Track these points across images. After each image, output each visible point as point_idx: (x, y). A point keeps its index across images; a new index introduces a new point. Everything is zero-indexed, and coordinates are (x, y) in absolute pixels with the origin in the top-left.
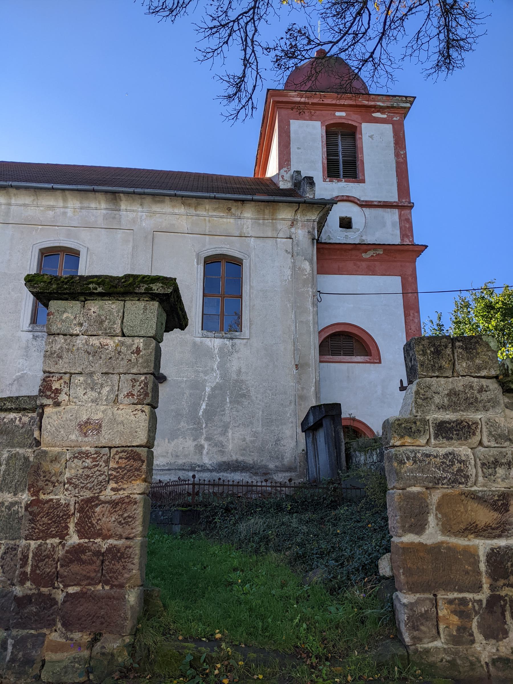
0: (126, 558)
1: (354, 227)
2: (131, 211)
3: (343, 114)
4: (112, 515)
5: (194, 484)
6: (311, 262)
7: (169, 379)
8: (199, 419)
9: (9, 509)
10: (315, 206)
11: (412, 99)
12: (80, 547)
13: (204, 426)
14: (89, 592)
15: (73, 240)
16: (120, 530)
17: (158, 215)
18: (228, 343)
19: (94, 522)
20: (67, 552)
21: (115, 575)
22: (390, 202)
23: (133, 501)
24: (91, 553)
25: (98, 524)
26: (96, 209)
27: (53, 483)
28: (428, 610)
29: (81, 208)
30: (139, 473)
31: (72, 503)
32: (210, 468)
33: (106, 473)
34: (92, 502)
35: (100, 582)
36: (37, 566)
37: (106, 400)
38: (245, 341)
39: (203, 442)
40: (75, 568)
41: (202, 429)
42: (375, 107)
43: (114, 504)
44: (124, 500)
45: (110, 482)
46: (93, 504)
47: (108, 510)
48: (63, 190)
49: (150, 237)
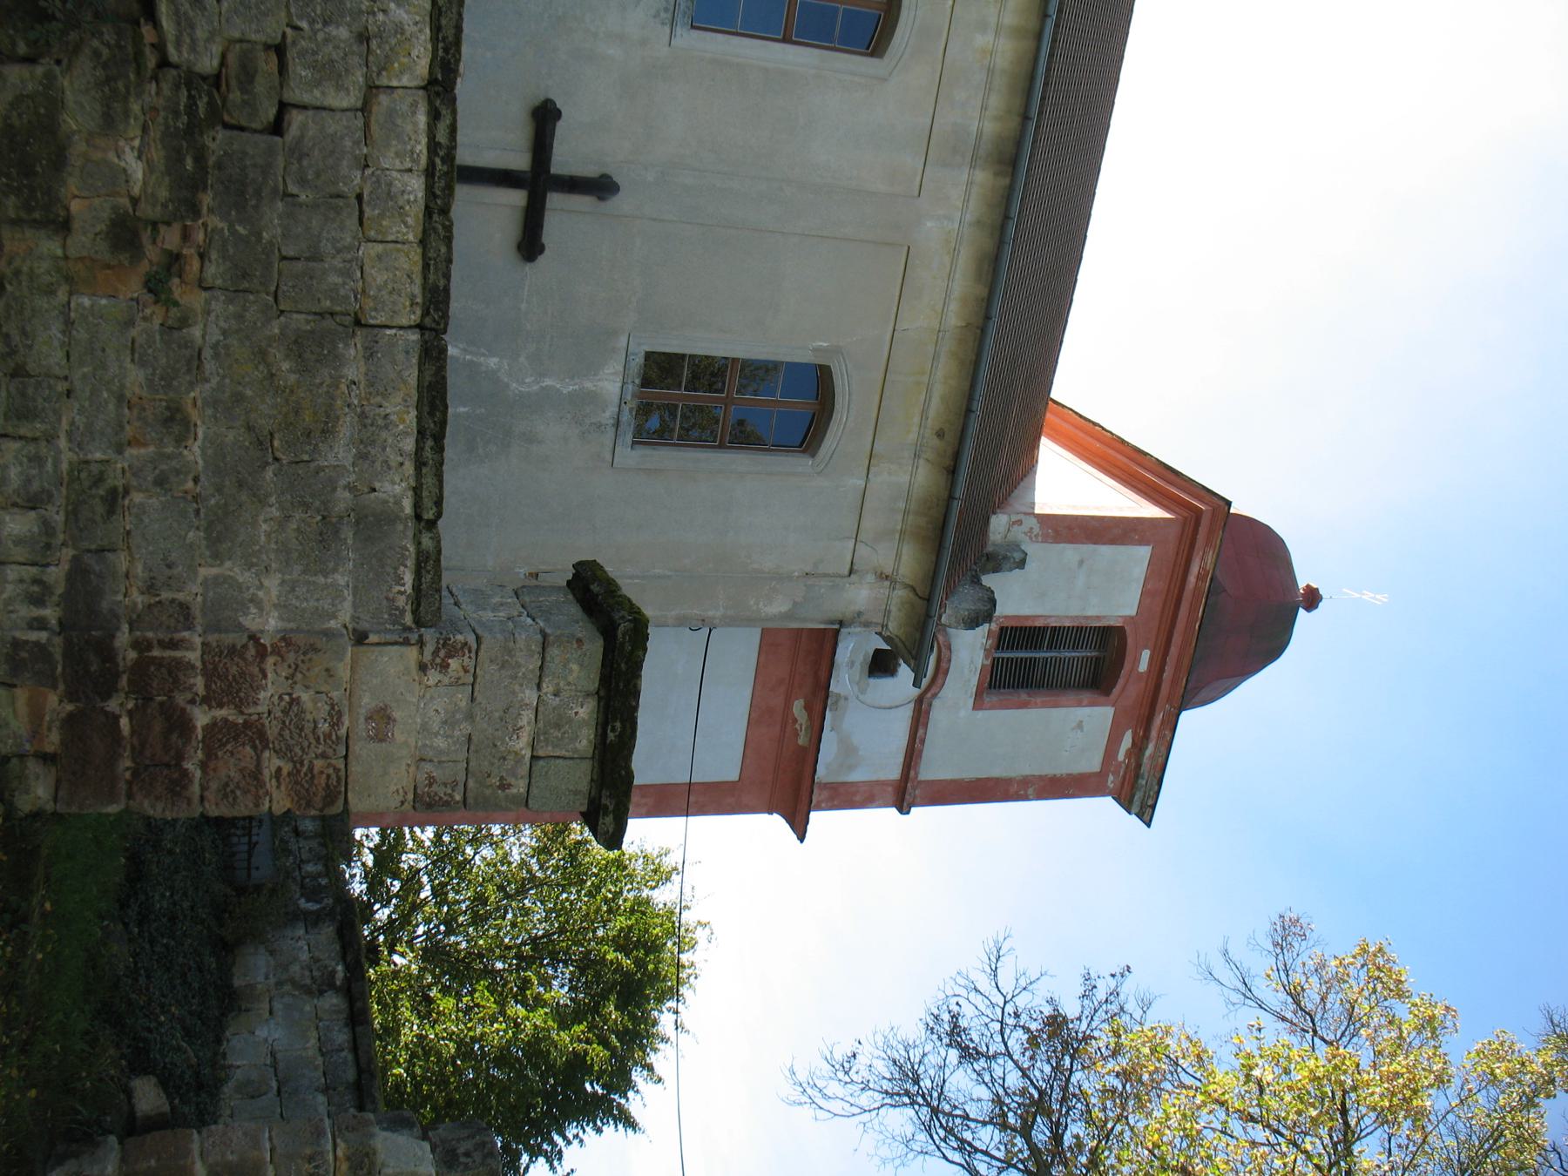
1: (872, 681)
2: (968, 193)
3: (1143, 666)
6: (787, 616)
7: (528, 267)
9: (251, 601)
10: (918, 635)
11: (1146, 817)
16: (214, 786)
17: (947, 260)
18: (608, 414)
20: (183, 710)
22: (917, 765)
26: (984, 108)
27: (293, 676)
29: (990, 71)
31: (260, 709)
36: (161, 665)
37: (425, 745)
38: (608, 457)
40: (158, 726)
42: (1146, 737)
43: (256, 775)
48: (1039, 37)
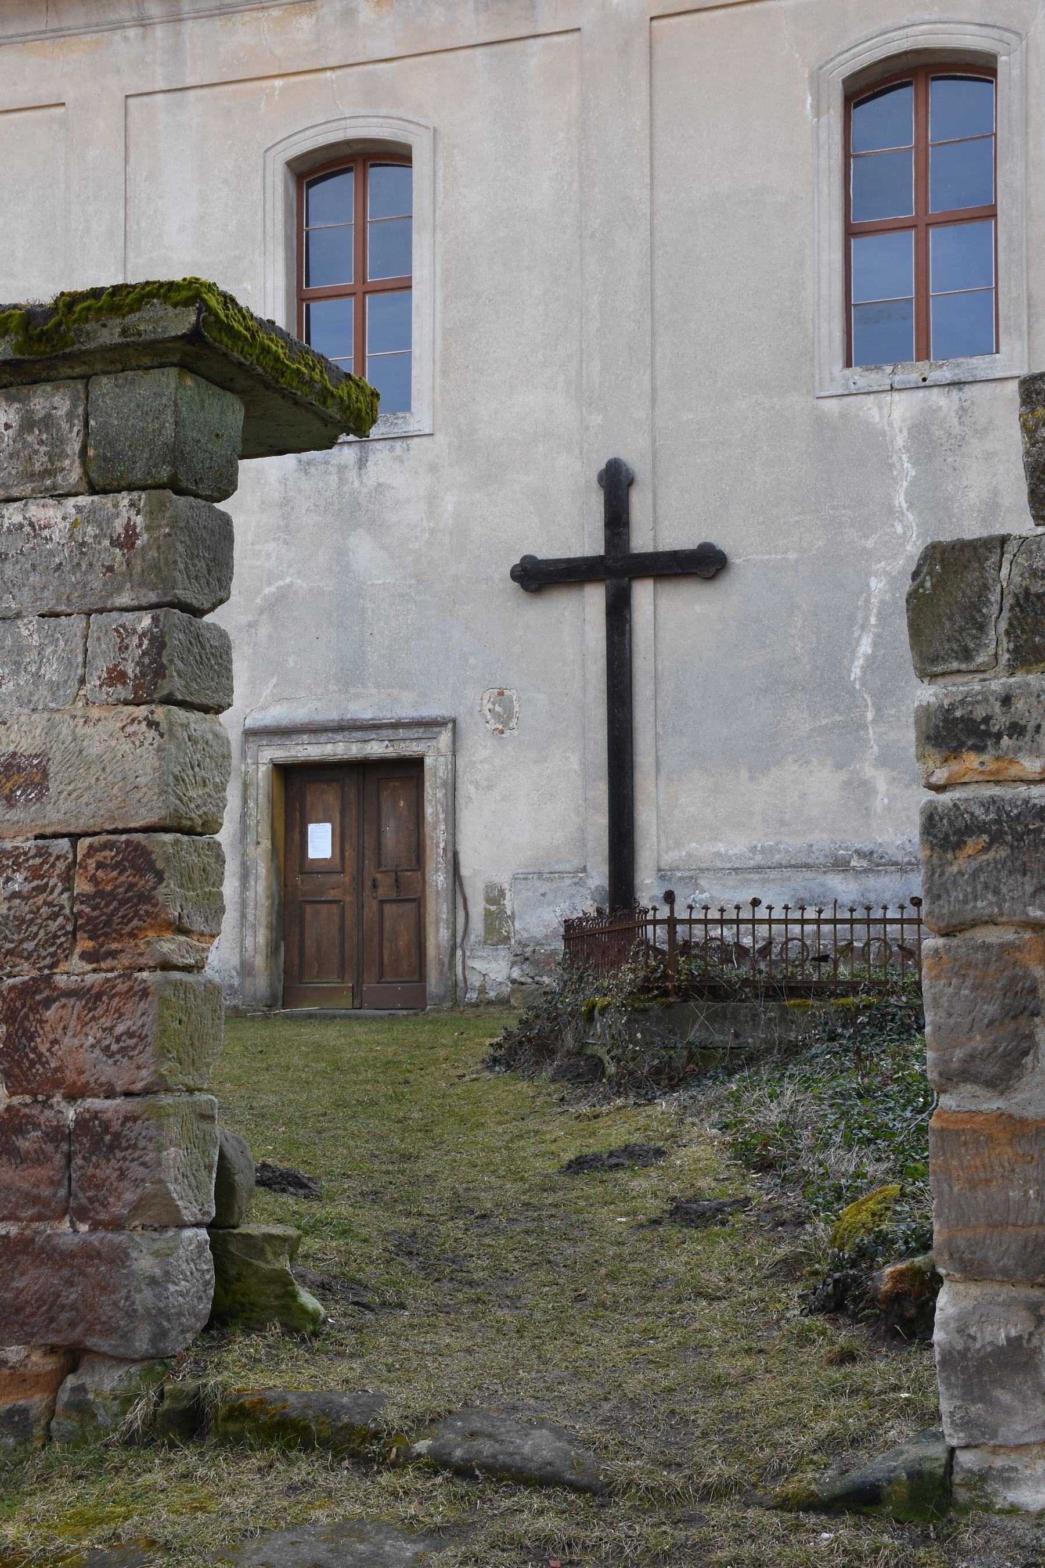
0: (126, 1149)
4: (86, 1029)
5: (672, 922)
7: (735, 560)
8: (852, 692)
12: (11, 1118)
13: (870, 715)
14: (39, 1240)
15: (383, 111)
16: (107, 1071)
19: (43, 1049)
21: (100, 1195)
23: (136, 988)
24: (39, 1133)
25: (52, 1053)
28: (1020, 1337)
30: (148, 907)
32: (899, 857)
33: (67, 911)
34: (35, 993)
35: (65, 1212)
39: (869, 771)
41: (865, 727)
44: (114, 987)
45: (79, 936)
46: (38, 998)
47: (75, 1016)
49: (640, 43)
